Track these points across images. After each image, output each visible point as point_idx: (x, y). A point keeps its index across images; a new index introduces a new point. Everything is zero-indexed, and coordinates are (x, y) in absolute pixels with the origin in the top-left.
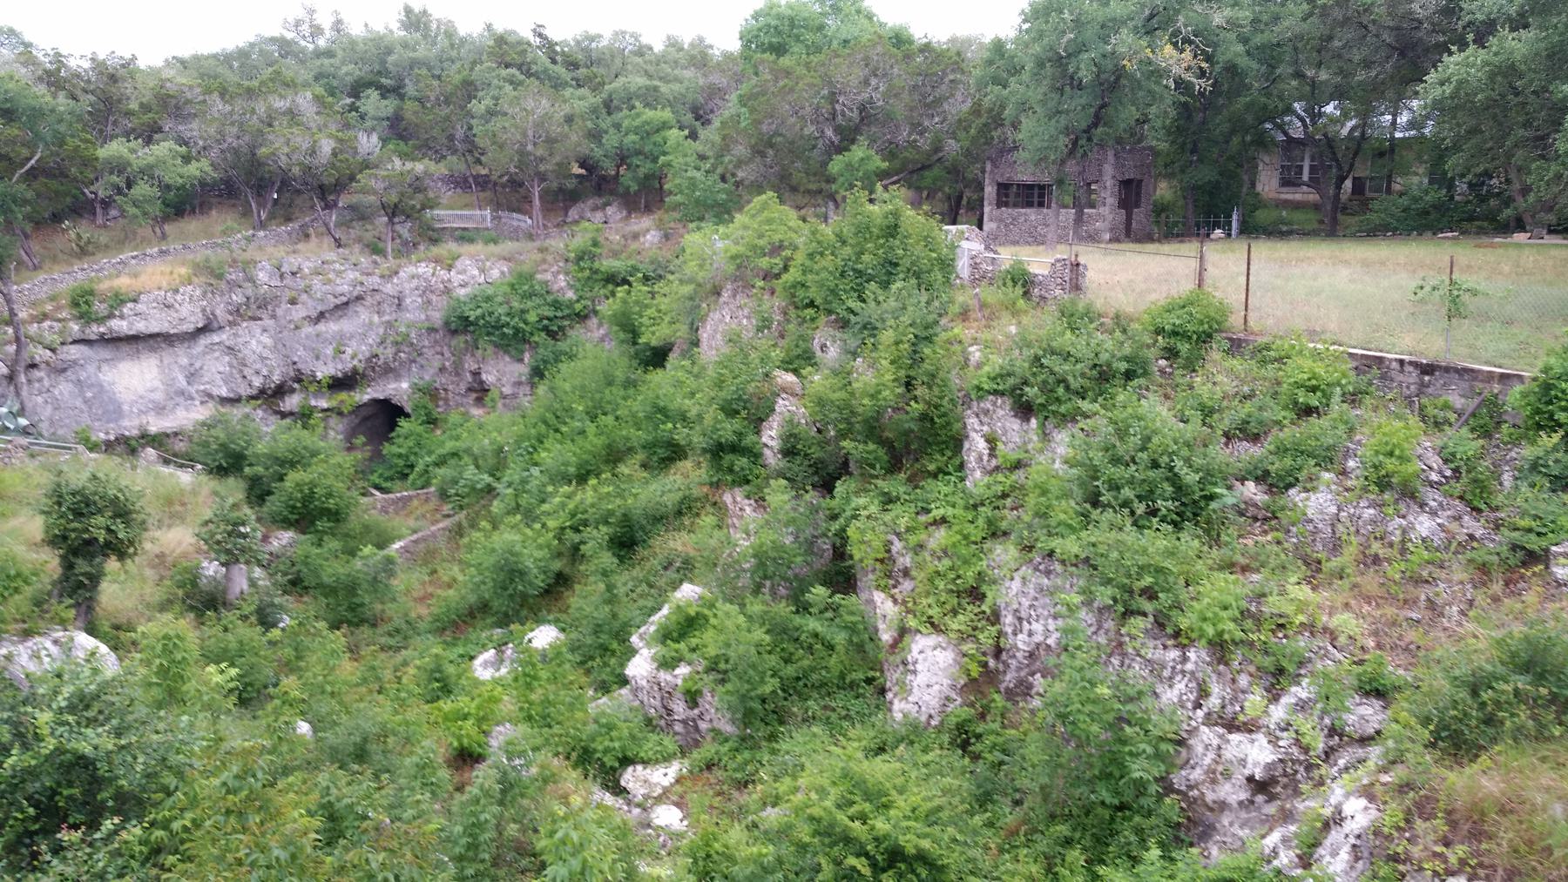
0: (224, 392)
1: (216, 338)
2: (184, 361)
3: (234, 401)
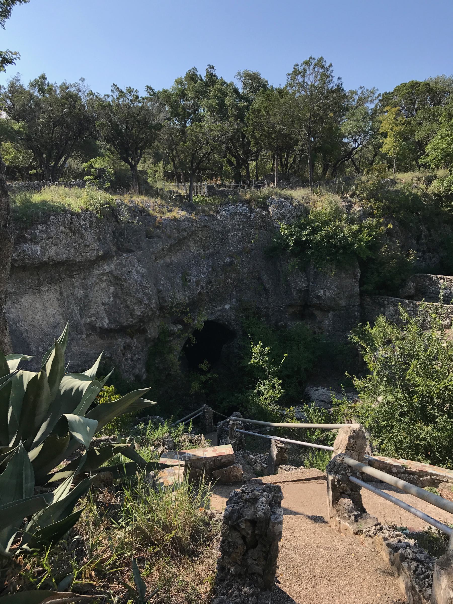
0: (106, 323)
1: (107, 268)
2: (80, 293)
3: (122, 330)
